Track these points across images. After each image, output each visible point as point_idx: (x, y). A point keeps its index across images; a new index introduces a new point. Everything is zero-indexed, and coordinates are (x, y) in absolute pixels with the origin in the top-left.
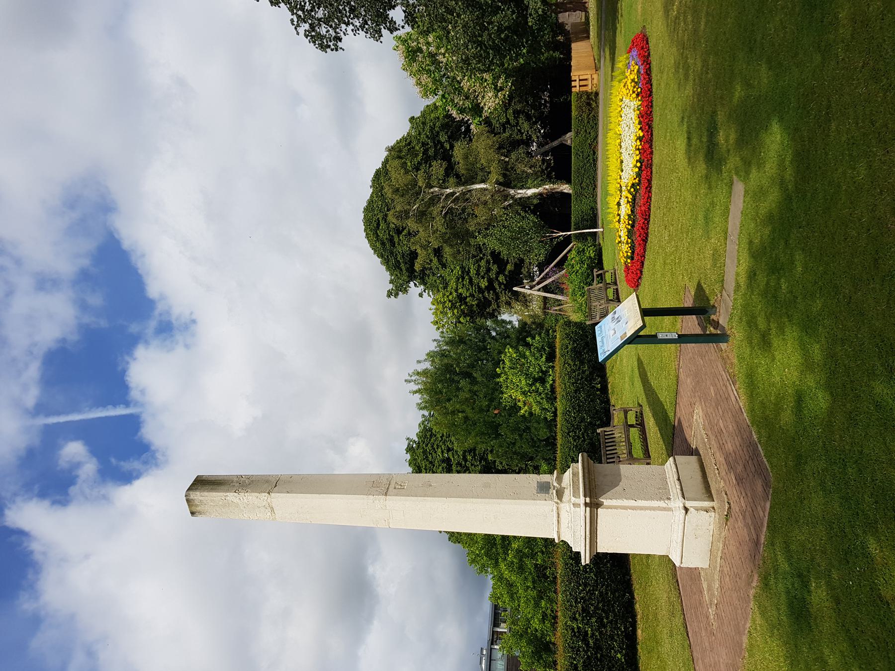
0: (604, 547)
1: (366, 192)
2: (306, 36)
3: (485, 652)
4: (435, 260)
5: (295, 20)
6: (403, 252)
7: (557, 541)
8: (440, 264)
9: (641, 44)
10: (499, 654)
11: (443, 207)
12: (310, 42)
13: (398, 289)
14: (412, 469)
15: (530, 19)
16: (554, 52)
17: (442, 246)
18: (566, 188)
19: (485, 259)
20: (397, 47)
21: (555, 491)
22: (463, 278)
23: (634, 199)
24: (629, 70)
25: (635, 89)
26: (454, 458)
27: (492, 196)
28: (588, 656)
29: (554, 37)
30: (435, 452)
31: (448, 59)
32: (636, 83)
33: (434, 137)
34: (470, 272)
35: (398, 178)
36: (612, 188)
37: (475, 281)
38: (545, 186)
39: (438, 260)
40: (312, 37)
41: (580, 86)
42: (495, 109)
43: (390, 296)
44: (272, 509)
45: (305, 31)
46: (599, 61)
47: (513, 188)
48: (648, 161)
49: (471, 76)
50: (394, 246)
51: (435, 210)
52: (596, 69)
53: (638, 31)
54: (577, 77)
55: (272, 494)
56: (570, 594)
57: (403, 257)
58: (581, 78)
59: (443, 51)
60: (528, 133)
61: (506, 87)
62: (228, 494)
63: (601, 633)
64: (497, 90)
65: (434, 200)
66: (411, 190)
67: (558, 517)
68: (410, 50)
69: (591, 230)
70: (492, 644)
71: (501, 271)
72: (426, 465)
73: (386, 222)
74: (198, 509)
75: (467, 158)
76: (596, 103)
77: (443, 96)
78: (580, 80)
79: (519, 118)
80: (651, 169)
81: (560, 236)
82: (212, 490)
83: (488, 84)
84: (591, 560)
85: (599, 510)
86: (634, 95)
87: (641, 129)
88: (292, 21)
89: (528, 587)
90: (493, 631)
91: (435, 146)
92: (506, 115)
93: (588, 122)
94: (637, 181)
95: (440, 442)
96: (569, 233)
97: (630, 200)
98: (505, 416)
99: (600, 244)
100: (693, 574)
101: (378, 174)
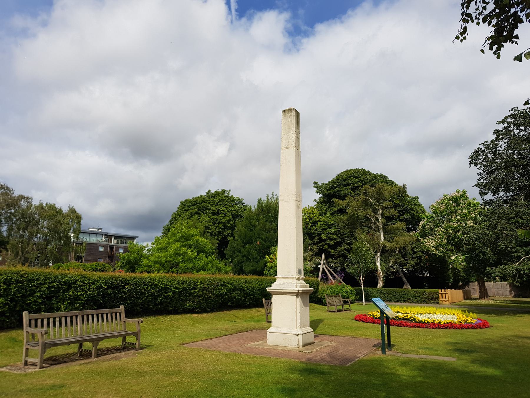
0: (275, 299)
1: (374, 171)
2: (478, 149)
3: (100, 230)
4: (336, 209)
5: (488, 143)
6: (340, 191)
7: (276, 277)
8: (333, 212)
9: (483, 325)
10: (99, 239)
11: (371, 215)
12: (475, 150)
13: (319, 188)
14: (213, 192)
15: (490, 268)
16: (453, 280)
17: (347, 214)
18: (380, 285)
19: (337, 238)
20: (459, 192)
21: (299, 277)
22: (326, 225)
23: (407, 319)
24: (471, 318)
25: (463, 321)
26: (221, 217)
27: (377, 243)
28: (187, 290)
29: (462, 280)
30: (223, 206)
31: (454, 220)
32: (466, 322)
33: (407, 210)
34: (330, 229)
35: (388, 191)
36: (408, 310)
37: (325, 232)
38: (381, 273)
39: (336, 211)
40: (478, 152)
41: (442, 294)
42: (425, 246)
44: (287, 148)
45: (481, 148)
46: (457, 305)
47: (381, 255)
48: (429, 326)
49: (445, 233)
50: (344, 186)
51: (369, 211)
52: (452, 303)
53: (490, 324)
54: (447, 293)
55: (295, 149)
56: (210, 281)
57: (337, 191)
58: (447, 295)
59: (458, 217)
60: (408, 264)
61: (438, 252)
62: (295, 128)
63: (195, 296)
64: (437, 247)
65: (375, 211)
66: (380, 197)
67: (289, 278)
68: (458, 199)
69: (364, 298)
70: (105, 235)
71: (330, 246)
73: (358, 182)
74: (287, 114)
75: (397, 229)
76: (433, 303)
77: (432, 217)
78: (445, 294)
79: (417, 259)
80: (425, 328)
81: (361, 281)
82: (296, 121)
83: (440, 242)
84: (269, 292)
85: (295, 296)
86: (460, 320)
87: (445, 323)
88: (487, 142)
90: (112, 236)
91: (402, 211)
92: (419, 252)
93: (422, 298)
94: (417, 321)
96: (362, 286)
97: (406, 317)
98: (256, 248)
99: (355, 303)
100: (264, 338)
101: (385, 178)
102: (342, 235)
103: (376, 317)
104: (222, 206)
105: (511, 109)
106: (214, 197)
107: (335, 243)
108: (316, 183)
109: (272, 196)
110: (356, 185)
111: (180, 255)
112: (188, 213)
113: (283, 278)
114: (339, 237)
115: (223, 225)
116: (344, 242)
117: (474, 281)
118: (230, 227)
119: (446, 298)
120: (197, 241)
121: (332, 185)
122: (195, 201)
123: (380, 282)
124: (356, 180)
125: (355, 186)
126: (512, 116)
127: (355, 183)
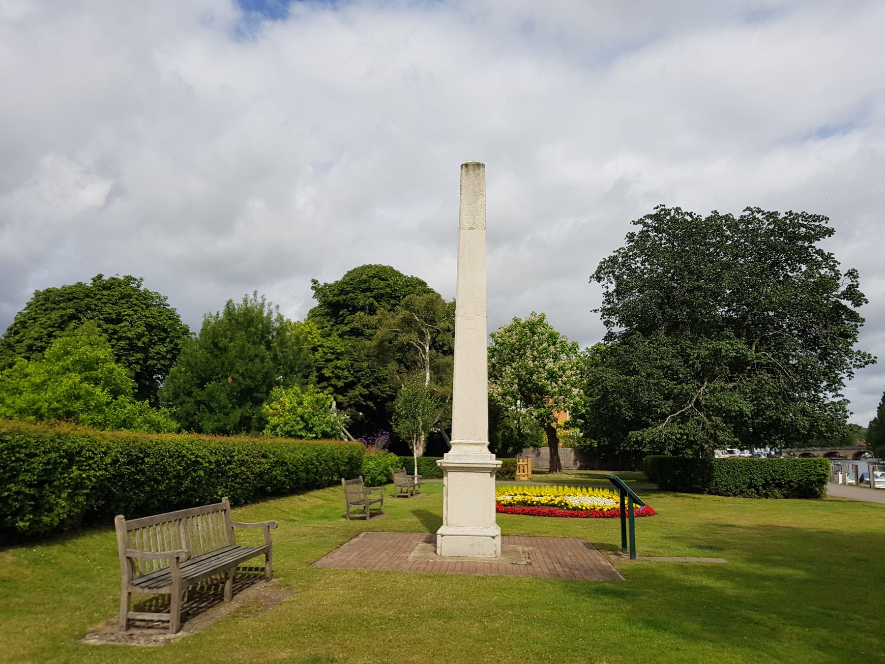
4: (347, 328)
19: (349, 375)
23: (554, 505)
30: (129, 308)
39: (348, 331)
43: (312, 282)
51: (414, 336)
57: (351, 299)
58: (526, 467)
65: (422, 335)
72: (113, 296)
73: (386, 286)
74: (471, 171)
83: (508, 388)
85: (489, 474)
87: (608, 510)
89: (50, 404)
94: (571, 507)
95: (141, 314)
101: (423, 284)
102: (357, 372)
103: (502, 502)
104: (125, 306)
105: (656, 207)
106: (109, 289)
107: (345, 383)
108: (315, 282)
109: (253, 298)
110: (382, 291)
111: (78, 397)
112: (55, 315)
113: (464, 444)
114: (352, 374)
115: (127, 342)
116: (359, 382)
117: (529, 445)
118: (142, 347)
119: (524, 472)
120: (111, 371)
121: (343, 288)
122: (69, 294)
123: (420, 448)
124: (382, 284)
125: (380, 294)
126: (656, 217)
127: (381, 289)
